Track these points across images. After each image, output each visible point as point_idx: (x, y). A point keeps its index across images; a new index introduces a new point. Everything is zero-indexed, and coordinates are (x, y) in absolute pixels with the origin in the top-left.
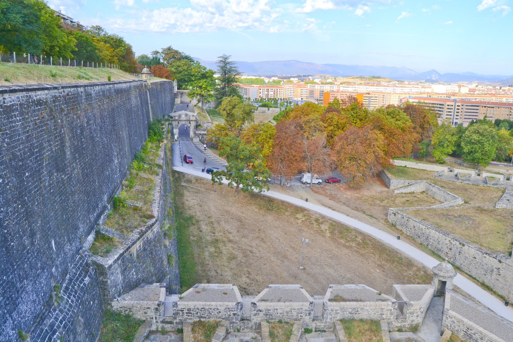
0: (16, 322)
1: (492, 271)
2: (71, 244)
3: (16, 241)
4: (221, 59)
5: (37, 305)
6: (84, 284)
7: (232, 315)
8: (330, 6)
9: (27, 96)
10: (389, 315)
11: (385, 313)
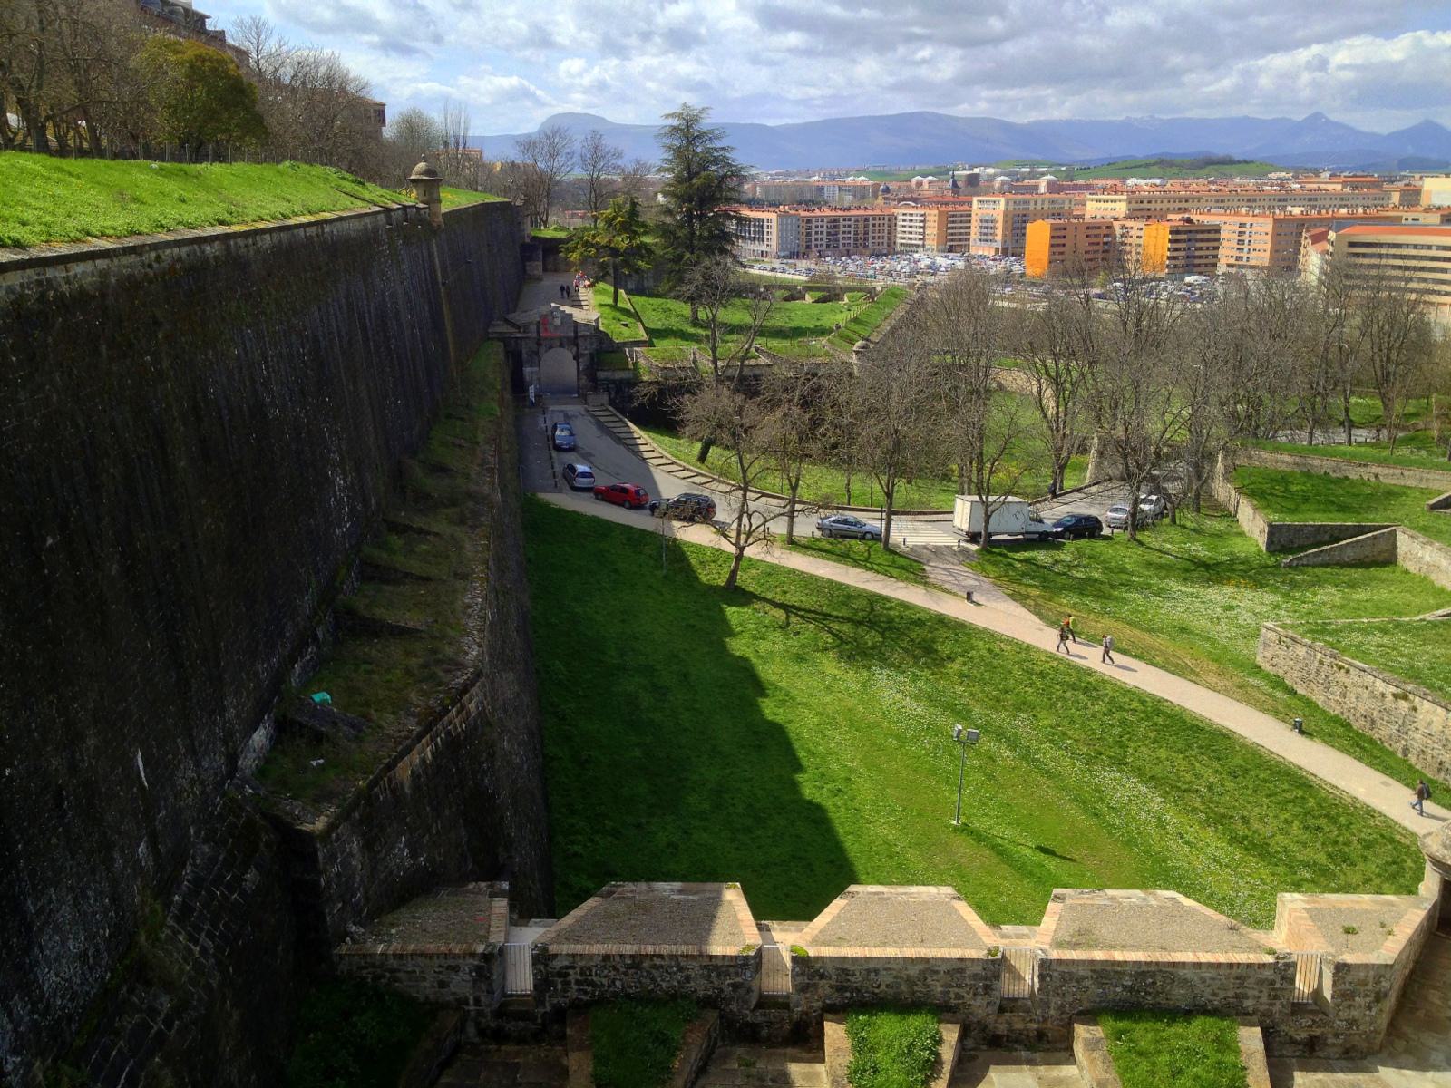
0: (22, 1029)
2: (198, 764)
3: (21, 762)
4: (676, 122)
5: (91, 969)
6: (243, 894)
7: (728, 990)
9: (39, 283)
10: (1264, 999)
11: (1250, 993)
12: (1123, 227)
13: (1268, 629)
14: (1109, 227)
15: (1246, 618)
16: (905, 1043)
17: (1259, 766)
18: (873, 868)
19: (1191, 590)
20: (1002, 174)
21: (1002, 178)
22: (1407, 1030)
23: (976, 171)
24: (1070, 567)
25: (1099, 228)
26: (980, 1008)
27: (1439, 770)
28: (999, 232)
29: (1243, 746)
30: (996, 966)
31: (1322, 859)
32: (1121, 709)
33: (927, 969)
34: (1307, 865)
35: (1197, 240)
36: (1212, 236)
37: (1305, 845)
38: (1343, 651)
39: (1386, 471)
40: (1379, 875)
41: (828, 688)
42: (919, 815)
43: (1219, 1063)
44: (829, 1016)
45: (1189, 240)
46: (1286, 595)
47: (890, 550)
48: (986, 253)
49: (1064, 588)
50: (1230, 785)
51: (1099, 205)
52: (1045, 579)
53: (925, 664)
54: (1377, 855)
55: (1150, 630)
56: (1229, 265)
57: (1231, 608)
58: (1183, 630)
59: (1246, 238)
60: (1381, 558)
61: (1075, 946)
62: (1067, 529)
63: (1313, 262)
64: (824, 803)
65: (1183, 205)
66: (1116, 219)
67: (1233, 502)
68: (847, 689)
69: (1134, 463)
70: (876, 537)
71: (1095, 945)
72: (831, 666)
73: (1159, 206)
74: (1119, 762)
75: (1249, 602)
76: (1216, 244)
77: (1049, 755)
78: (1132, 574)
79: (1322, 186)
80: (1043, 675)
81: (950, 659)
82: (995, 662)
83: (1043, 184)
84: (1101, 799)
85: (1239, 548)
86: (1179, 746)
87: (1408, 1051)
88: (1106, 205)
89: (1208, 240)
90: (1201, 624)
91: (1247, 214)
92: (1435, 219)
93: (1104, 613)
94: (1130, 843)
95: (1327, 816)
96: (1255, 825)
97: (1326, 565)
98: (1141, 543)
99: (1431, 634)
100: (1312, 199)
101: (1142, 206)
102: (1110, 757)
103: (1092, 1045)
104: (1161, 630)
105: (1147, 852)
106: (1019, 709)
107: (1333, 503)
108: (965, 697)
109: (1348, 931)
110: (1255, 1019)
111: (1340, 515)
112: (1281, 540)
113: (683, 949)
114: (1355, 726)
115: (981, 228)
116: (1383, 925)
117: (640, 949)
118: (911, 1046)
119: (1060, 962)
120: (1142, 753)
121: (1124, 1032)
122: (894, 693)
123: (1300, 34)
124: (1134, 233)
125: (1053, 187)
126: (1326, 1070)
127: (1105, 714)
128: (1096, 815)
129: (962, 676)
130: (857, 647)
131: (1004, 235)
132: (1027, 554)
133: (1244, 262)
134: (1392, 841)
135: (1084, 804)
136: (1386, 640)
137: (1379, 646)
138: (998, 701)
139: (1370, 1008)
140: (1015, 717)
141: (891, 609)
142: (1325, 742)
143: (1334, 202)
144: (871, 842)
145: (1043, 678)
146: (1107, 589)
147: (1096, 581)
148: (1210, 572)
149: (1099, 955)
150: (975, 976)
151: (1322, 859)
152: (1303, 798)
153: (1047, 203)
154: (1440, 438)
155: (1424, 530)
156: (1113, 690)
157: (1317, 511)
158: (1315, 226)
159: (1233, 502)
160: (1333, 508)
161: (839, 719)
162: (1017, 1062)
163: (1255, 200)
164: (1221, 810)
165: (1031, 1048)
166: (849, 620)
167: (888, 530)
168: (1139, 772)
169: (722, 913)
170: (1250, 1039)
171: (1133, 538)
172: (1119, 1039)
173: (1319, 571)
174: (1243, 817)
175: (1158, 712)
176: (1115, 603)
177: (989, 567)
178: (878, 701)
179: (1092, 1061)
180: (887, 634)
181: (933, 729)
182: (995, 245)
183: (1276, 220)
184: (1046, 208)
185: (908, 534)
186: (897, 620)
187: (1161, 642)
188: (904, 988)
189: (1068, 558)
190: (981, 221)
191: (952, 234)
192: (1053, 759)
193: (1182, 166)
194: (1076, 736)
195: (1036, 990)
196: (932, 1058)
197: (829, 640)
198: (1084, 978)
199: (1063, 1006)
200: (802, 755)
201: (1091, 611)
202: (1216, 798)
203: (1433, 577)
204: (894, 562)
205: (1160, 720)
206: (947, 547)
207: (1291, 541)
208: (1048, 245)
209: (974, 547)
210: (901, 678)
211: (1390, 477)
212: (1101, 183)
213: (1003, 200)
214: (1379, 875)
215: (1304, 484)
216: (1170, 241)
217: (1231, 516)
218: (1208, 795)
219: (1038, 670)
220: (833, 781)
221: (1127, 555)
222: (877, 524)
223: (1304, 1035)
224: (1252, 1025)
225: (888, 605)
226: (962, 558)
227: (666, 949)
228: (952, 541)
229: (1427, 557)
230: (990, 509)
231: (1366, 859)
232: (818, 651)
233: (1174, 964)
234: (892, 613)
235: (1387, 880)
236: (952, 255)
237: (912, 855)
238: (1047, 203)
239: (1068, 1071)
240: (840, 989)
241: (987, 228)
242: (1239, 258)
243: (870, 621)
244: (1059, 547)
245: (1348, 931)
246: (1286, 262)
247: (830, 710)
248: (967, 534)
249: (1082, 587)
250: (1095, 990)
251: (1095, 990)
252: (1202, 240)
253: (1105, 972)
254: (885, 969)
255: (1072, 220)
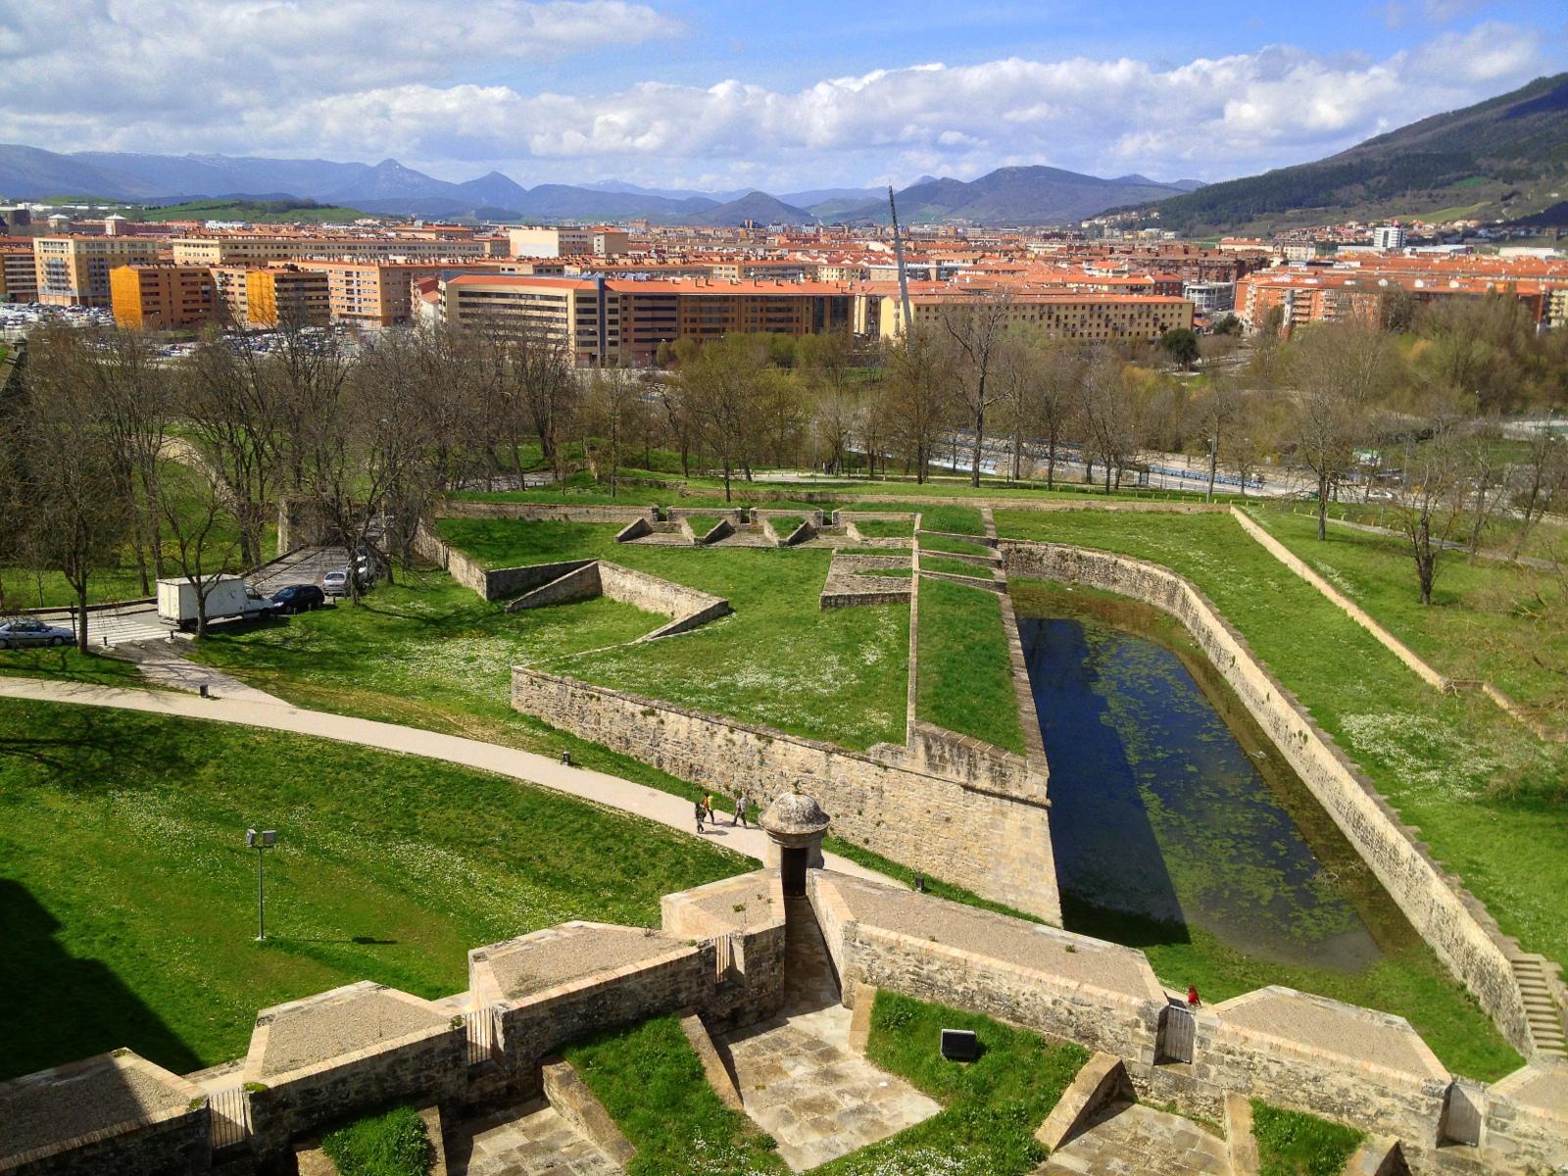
1: (863, 798)
8: (647, 21)
10: (695, 988)
11: (683, 986)
12: (221, 274)
13: (519, 672)
14: (207, 274)
15: (489, 667)
16: (393, 1142)
17: (543, 804)
18: (182, 1013)
19: (428, 648)
20: (55, 212)
21: (57, 216)
22: (796, 981)
23: (21, 207)
24: (303, 642)
25: (195, 275)
26: (451, 1082)
27: (690, 773)
28: (73, 278)
29: (524, 788)
30: (458, 1036)
31: (618, 876)
32: (400, 778)
33: (394, 1062)
34: (606, 885)
35: (305, 289)
36: (320, 284)
37: (600, 867)
38: (590, 681)
39: (574, 510)
40: (668, 878)
41: (60, 826)
42: (217, 941)
43: (677, 1056)
44: (299, 1146)
45: (297, 289)
46: (517, 639)
47: (88, 652)
48: (60, 303)
49: (302, 666)
50: (521, 829)
51: (187, 250)
52: (279, 659)
53: (171, 775)
54: (662, 860)
55: (403, 694)
56: (342, 316)
57: (472, 659)
58: (435, 688)
59: (354, 286)
60: (589, 593)
61: (529, 991)
62: (288, 602)
63: (427, 309)
64: (100, 958)
65: (282, 251)
66: (213, 265)
67: (442, 555)
68: (85, 823)
69: (336, 528)
70: (67, 640)
71: (544, 985)
72: (56, 801)
73: (256, 252)
74: (411, 833)
75: (490, 651)
76: (325, 293)
77: (339, 843)
78: (366, 640)
79: (417, 235)
80: (310, 760)
81: (201, 763)
82: (254, 758)
83: (109, 225)
84: (406, 875)
85: (462, 600)
86: (466, 802)
87: (803, 999)
88: (196, 250)
89: (317, 289)
90: (450, 679)
91: (352, 263)
92: (527, 269)
93: (352, 685)
94: (444, 909)
95: (613, 835)
96: (553, 861)
97: (544, 605)
98: (367, 608)
99: (655, 652)
100: (411, 247)
101: (237, 251)
102: (400, 830)
103: (565, 1081)
104: (414, 692)
105: (463, 913)
106: (293, 803)
107: (536, 546)
108: (229, 802)
109: (738, 909)
110: (690, 1008)
111: (545, 556)
112: (500, 587)
113: (117, 1129)
114: (613, 748)
115: (790, 320)
116: (760, 898)
117: (63, 1146)
118: (400, 1143)
119: (521, 1010)
120: (431, 818)
121: (591, 1057)
122: (145, 815)
123: (357, 78)
124: (235, 281)
125: (121, 227)
126: (751, 1036)
127: (386, 788)
128: (403, 891)
129: (219, 780)
130: (83, 771)
131: (80, 283)
132: (253, 636)
133: (356, 312)
134: (671, 844)
135: (388, 883)
136: (622, 665)
137: (619, 671)
138: (267, 798)
139: (773, 970)
140: (290, 811)
141: (113, 720)
142: (593, 769)
143: (432, 252)
144: (171, 985)
145: (311, 763)
146: (347, 659)
147: (334, 653)
148: (444, 626)
149: (554, 992)
150: (444, 1052)
151: (618, 876)
152: (589, 824)
153: (126, 245)
154: (600, 477)
155: (619, 561)
156: (388, 761)
157: (525, 554)
158: (421, 276)
159: (442, 555)
160: (538, 550)
161: (87, 859)
162: (497, 1123)
163: (355, 248)
164: (519, 855)
165: (504, 1106)
166: (63, 742)
167: (84, 630)
168: (433, 837)
169: (133, 1080)
170: (693, 1027)
171: (357, 604)
172: (588, 1066)
173: (540, 611)
174: (540, 856)
175: (438, 773)
176: (360, 673)
177: (214, 656)
178: (128, 828)
179: (571, 1095)
180: (116, 749)
181: (203, 846)
182: (69, 293)
183: (382, 269)
184: (126, 252)
185: (107, 632)
186: (125, 732)
187: (417, 704)
188: (374, 1089)
189: (298, 634)
190: (48, 265)
191: (13, 281)
192: (344, 846)
193: (263, 209)
194: (361, 817)
195: (501, 1046)
196: (425, 1146)
197: (44, 771)
198: (544, 1019)
199: (528, 1053)
200: (53, 909)
201: (339, 685)
202: (512, 844)
203: (636, 603)
204: (98, 666)
205: (441, 781)
206: (158, 640)
207: (509, 587)
208: (138, 294)
209: (190, 636)
210: (147, 797)
211: (578, 516)
212: (176, 225)
213: (71, 242)
214: (668, 878)
215: (504, 530)
216: (277, 290)
217: (443, 570)
218: (504, 843)
219: (302, 756)
220: (103, 931)
221: (360, 624)
222: (68, 625)
223: (728, 1011)
224: (690, 1015)
225: (108, 716)
226: (179, 650)
227: (97, 1136)
228: (162, 633)
229: (629, 586)
230: (204, 590)
231: (654, 866)
232: (33, 786)
233: (619, 980)
234: (116, 725)
235: (676, 881)
236: (17, 305)
237: (222, 987)
238: (126, 245)
239: (547, 1114)
240: (306, 1113)
241: (57, 274)
242: (349, 308)
243: (90, 739)
244: (285, 623)
245: (738, 909)
246: (399, 315)
247: (71, 851)
248: (178, 622)
249: (322, 661)
250: (554, 1027)
251: (554, 1027)
252: (311, 289)
253: (560, 1007)
254: (353, 1075)
255: (163, 266)
